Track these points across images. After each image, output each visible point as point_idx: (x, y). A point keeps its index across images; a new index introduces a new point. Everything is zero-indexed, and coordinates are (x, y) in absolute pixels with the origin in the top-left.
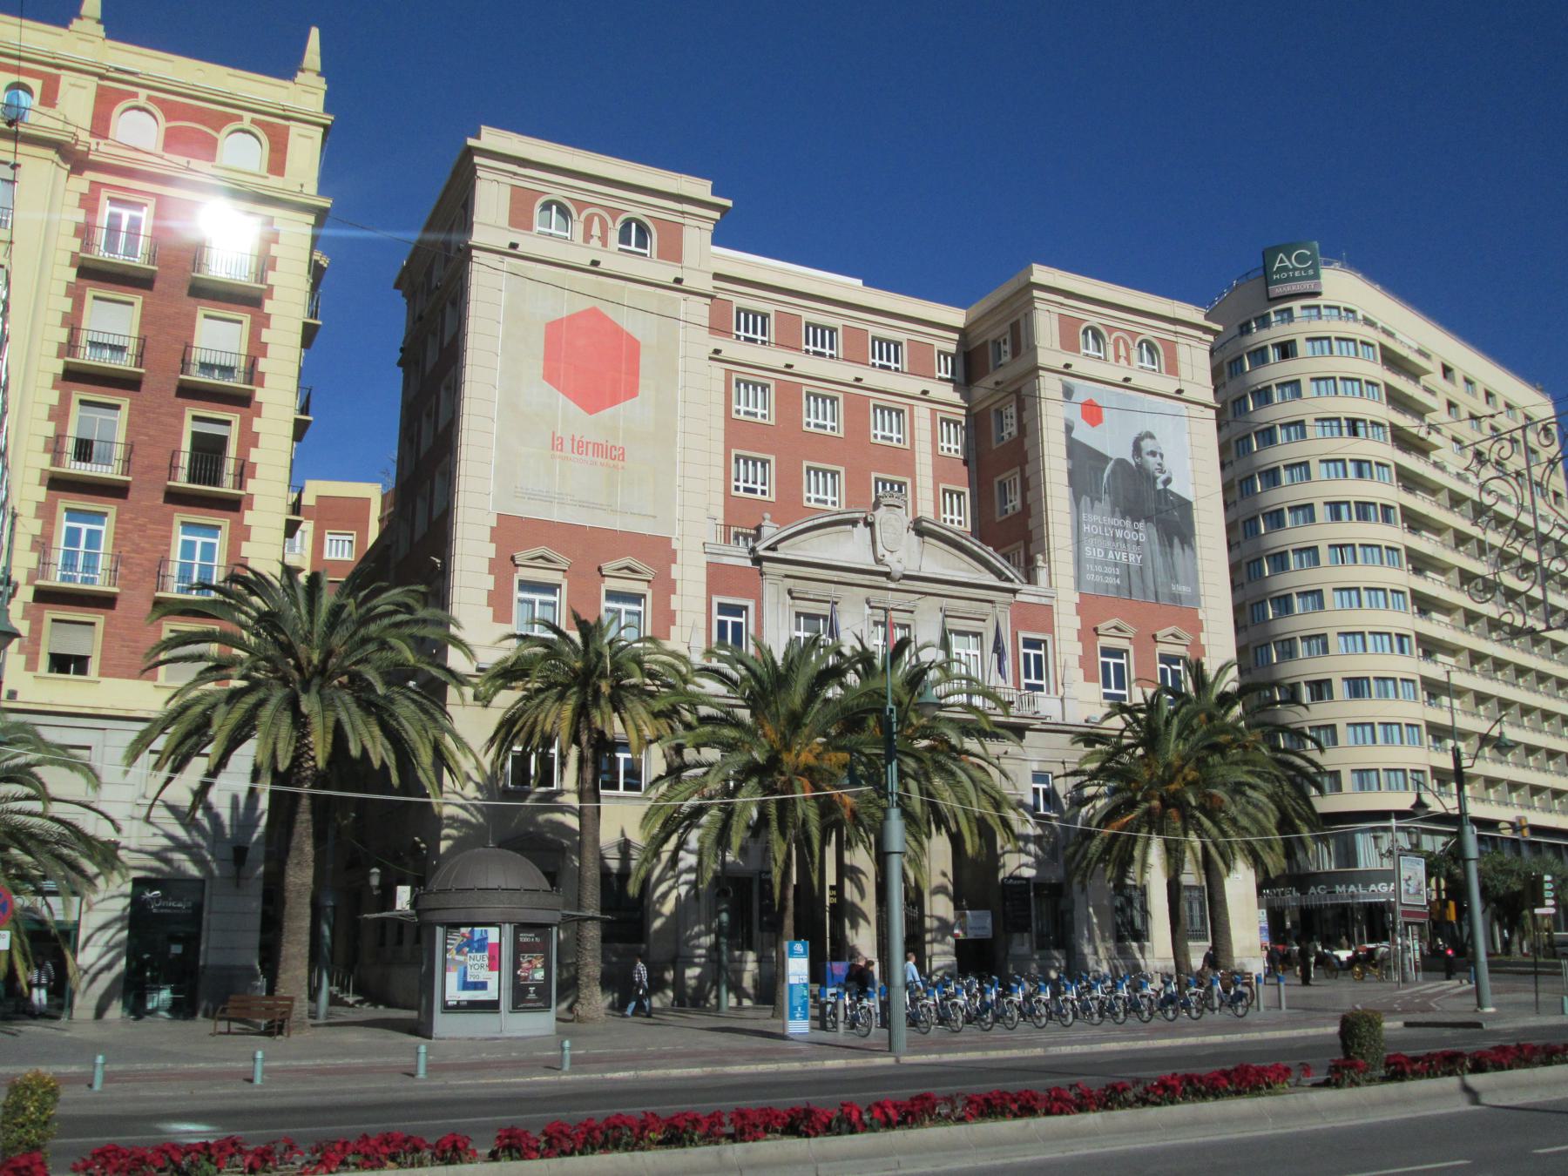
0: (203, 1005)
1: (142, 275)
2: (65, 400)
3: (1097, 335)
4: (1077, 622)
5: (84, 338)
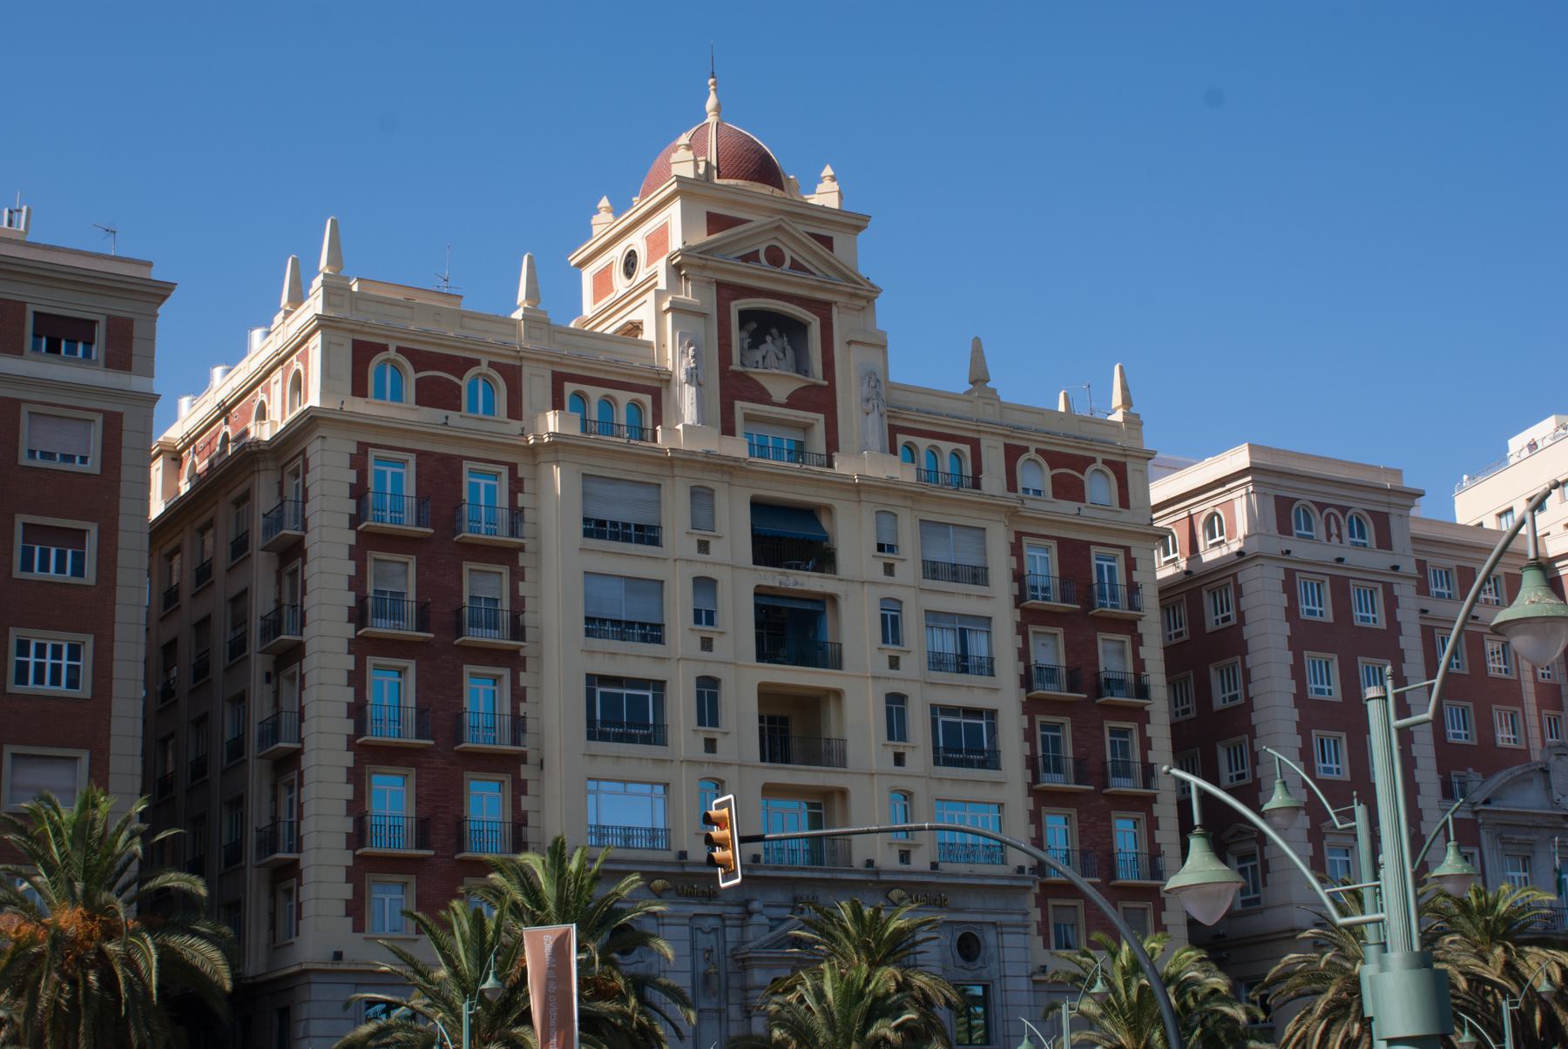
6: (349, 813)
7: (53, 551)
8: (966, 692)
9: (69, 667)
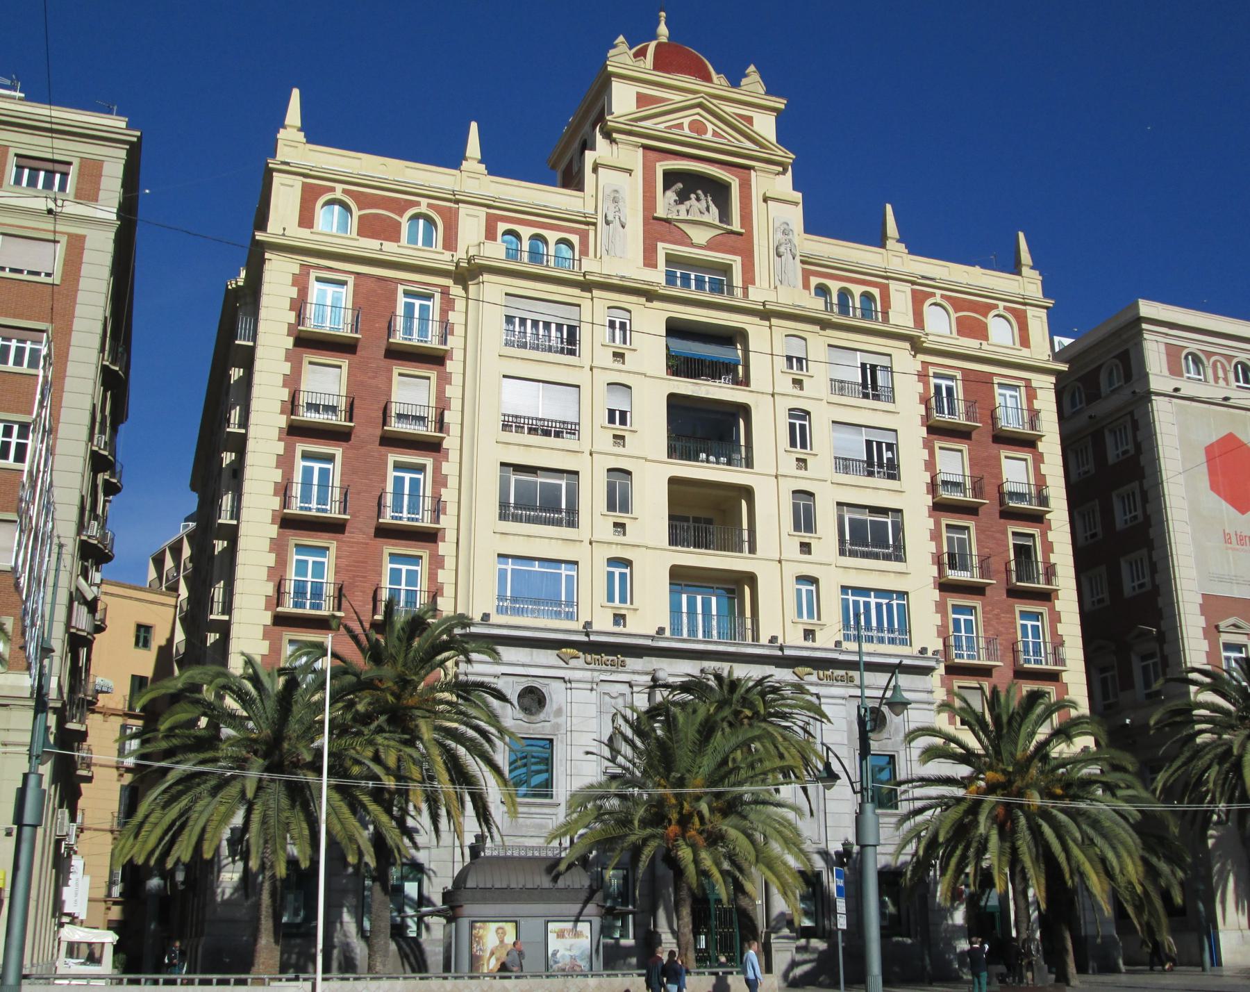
0: (1091, 964)
1: (962, 428)
2: (290, 451)
3: (1197, 361)
4: (1202, 622)
5: (303, 399)
6: (269, 579)
7: (699, 598)
8: (876, 492)
9: (18, 444)
